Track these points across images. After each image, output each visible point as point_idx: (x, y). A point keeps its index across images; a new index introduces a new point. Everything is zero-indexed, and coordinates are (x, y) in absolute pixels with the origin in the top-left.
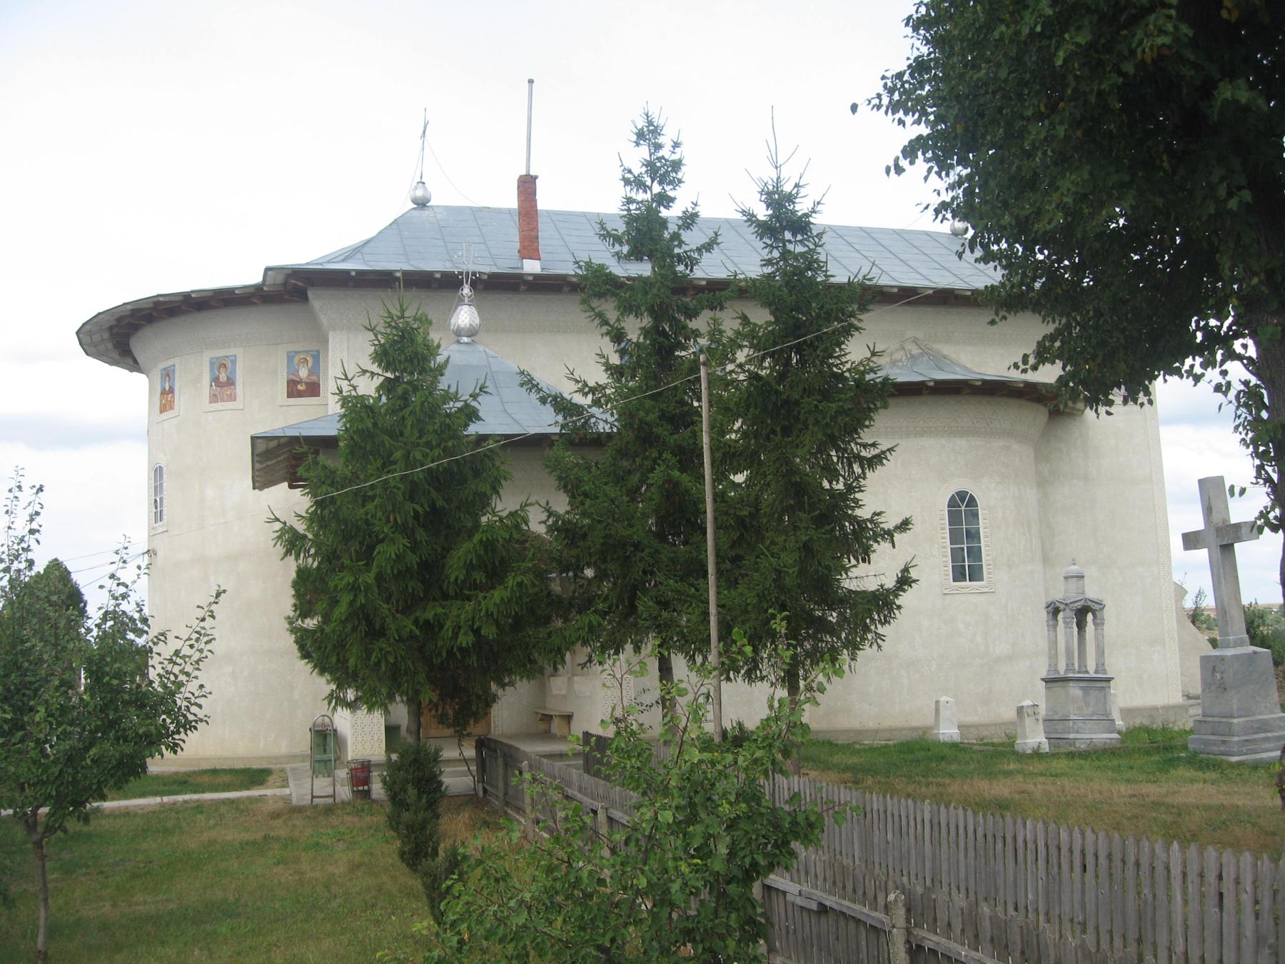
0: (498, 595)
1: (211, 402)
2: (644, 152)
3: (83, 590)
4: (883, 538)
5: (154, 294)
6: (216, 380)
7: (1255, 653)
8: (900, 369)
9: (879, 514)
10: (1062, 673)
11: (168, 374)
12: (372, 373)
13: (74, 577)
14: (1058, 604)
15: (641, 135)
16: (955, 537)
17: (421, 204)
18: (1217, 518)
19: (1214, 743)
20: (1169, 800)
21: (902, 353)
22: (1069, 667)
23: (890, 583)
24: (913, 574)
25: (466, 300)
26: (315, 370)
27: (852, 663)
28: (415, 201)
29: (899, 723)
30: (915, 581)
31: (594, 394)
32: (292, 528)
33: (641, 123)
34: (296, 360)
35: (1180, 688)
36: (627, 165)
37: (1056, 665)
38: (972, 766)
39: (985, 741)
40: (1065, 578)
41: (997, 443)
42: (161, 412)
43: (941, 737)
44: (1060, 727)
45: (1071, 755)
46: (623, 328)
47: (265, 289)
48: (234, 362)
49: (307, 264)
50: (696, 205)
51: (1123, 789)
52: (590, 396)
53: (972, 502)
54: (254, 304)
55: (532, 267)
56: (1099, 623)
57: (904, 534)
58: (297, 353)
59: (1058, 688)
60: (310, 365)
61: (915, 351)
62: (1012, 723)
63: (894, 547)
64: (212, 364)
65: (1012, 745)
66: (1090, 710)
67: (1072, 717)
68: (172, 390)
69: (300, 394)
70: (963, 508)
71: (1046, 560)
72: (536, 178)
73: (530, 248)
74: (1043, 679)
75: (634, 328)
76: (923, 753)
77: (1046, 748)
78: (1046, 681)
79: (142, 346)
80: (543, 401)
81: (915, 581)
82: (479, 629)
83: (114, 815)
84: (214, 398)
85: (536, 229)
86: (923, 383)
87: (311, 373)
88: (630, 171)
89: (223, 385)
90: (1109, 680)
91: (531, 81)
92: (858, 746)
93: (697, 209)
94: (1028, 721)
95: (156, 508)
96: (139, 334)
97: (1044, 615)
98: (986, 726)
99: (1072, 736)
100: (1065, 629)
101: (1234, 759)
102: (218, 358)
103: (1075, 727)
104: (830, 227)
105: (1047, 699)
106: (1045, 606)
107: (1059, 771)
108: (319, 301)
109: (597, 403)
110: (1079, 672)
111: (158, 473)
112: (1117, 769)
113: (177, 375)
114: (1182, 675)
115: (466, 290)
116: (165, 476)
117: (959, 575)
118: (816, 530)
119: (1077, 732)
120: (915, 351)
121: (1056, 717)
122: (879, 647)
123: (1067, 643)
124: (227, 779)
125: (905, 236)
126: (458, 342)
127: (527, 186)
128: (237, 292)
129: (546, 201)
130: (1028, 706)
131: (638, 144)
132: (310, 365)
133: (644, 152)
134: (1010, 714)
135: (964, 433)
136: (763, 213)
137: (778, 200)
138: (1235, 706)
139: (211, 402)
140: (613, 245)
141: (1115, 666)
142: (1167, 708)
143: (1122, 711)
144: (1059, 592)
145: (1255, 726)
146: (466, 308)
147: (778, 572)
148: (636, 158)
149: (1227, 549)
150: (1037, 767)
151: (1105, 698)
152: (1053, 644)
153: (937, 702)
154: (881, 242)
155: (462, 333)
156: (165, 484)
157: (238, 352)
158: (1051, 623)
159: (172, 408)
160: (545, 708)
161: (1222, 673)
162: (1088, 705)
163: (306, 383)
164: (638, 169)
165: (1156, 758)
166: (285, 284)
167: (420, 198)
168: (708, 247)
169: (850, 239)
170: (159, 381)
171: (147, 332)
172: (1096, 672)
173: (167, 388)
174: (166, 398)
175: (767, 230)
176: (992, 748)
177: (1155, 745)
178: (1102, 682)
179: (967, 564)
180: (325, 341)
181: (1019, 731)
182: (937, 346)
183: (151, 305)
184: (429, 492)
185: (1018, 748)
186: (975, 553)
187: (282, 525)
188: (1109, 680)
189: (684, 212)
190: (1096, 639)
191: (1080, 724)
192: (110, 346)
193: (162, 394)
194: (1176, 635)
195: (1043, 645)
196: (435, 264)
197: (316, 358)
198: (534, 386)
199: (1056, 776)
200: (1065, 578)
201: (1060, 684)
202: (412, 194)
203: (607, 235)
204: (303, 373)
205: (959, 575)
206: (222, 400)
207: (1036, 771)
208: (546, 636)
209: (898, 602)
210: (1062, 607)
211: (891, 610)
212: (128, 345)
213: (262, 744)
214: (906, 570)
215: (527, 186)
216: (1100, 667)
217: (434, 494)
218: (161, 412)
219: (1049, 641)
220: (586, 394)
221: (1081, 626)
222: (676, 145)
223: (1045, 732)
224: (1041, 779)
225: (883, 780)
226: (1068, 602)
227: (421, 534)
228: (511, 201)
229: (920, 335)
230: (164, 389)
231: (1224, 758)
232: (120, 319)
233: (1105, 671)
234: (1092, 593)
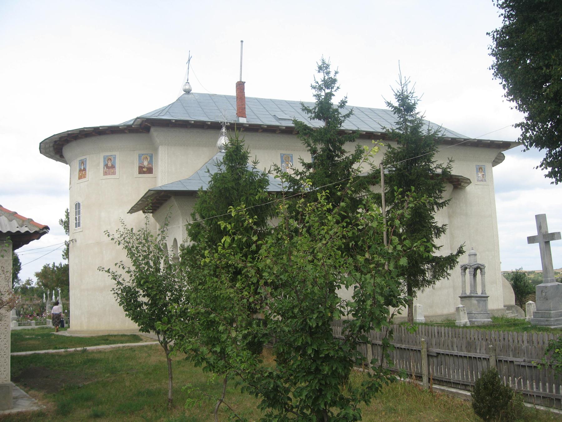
1: (104, 175)
3: (19, 258)
5: (83, 127)
6: (106, 165)
7: (559, 285)
9: (445, 225)
11: (83, 162)
15: (320, 68)
17: (188, 92)
18: (543, 230)
19: (543, 321)
23: (455, 253)
24: (464, 249)
26: (150, 162)
28: (185, 91)
31: (301, 175)
33: (320, 64)
34: (142, 157)
36: (317, 80)
40: (469, 255)
42: (79, 179)
43: (417, 321)
46: (316, 148)
47: (133, 126)
48: (115, 158)
49: (151, 116)
54: (125, 133)
55: (242, 120)
56: (482, 273)
58: (143, 155)
59: (466, 300)
60: (148, 160)
64: (104, 158)
67: (474, 312)
68: (85, 169)
69: (144, 173)
72: (245, 83)
73: (241, 112)
74: (459, 297)
75: (319, 147)
78: (461, 297)
79: (67, 152)
83: (93, 352)
84: (105, 173)
85: (244, 104)
87: (149, 163)
88: (317, 83)
89: (110, 168)
90: (487, 297)
91: (242, 42)
93: (347, 100)
95: (76, 221)
96: (69, 144)
101: (552, 327)
102: (107, 156)
104: (358, 108)
108: (155, 133)
109: (301, 178)
111: (78, 206)
113: (88, 162)
115: (224, 130)
116: (81, 207)
119: (475, 318)
122: (448, 278)
126: (220, 152)
127: (240, 86)
128: (120, 127)
129: (249, 93)
130: (461, 307)
131: (319, 72)
132: (148, 160)
136: (396, 104)
137: (403, 98)
138: (551, 306)
139: (104, 175)
145: (560, 314)
146: (223, 137)
148: (320, 77)
149: (547, 243)
152: (464, 282)
156: (81, 211)
157: (117, 154)
158: (463, 274)
159: (85, 177)
161: (546, 293)
163: (147, 168)
166: (140, 125)
167: (187, 89)
168: (348, 116)
169: (366, 113)
170: (78, 166)
171: (74, 144)
172: (482, 294)
173: (82, 168)
174: (82, 174)
175: (397, 110)
178: (484, 298)
180: (156, 150)
183: (78, 132)
188: (487, 297)
189: (341, 101)
191: (476, 315)
192: (52, 149)
194: (501, 280)
197: (151, 157)
198: (279, 171)
200: (469, 255)
201: (468, 298)
202: (184, 87)
203: (305, 109)
204: (146, 163)
206: (109, 174)
209: (458, 260)
210: (468, 267)
211: (454, 263)
212: (62, 149)
213: (127, 324)
214: (461, 247)
215: (240, 86)
216: (483, 291)
218: (79, 179)
220: (297, 175)
222: (336, 73)
228: (232, 92)
230: (81, 169)
231: (549, 327)
232: (61, 138)
234: (479, 262)
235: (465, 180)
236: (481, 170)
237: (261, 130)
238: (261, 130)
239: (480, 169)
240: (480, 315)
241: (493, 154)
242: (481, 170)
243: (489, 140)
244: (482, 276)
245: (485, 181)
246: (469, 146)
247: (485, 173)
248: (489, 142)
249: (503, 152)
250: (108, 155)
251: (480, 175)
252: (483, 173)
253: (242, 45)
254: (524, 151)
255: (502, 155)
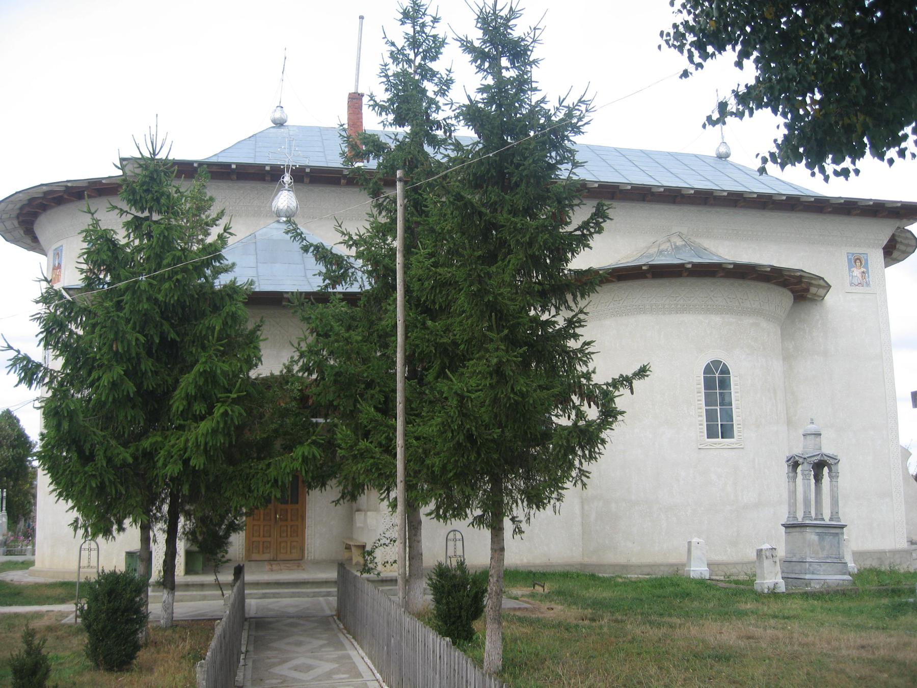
0: (205, 426)
2: (409, 28)
4: (622, 384)
8: (665, 256)
10: (800, 520)
12: (121, 210)
13: (22, 423)
14: (797, 458)
15: (406, 15)
16: (709, 401)
17: (279, 124)
20: (900, 656)
21: (668, 244)
22: (807, 514)
25: (287, 186)
27: (558, 504)
28: (274, 121)
29: (659, 559)
30: (622, 413)
32: (26, 358)
35: (905, 536)
37: (795, 512)
38: (711, 605)
39: (732, 578)
41: (748, 321)
44: (798, 567)
45: (806, 595)
50: (450, 71)
51: (852, 635)
52: (354, 248)
53: (725, 371)
56: (834, 476)
57: (642, 381)
59: (796, 533)
61: (679, 243)
62: (754, 563)
63: (632, 393)
65: (751, 582)
66: (825, 553)
68: (59, 267)
70: (717, 375)
71: (789, 423)
74: (783, 525)
76: (671, 589)
77: (782, 588)
78: (787, 526)
80: (306, 249)
81: (622, 413)
82: (189, 459)
86: (682, 265)
88: (393, 44)
90: (842, 527)
91: (362, 18)
92: (620, 580)
94: (767, 563)
97: (785, 468)
98: (735, 564)
99: (808, 577)
100: (804, 480)
103: (811, 568)
105: (787, 542)
106: (786, 459)
107: (792, 613)
110: (816, 519)
112: (848, 612)
114: (907, 524)
115: (287, 178)
117: (711, 434)
118: (507, 351)
119: (813, 573)
120: (679, 243)
121: (794, 559)
122: (584, 485)
123: (805, 492)
124: (59, 591)
125: (679, 157)
126: (278, 222)
130: (428, 594)
131: (403, 23)
133: (409, 28)
134: (753, 556)
135: (719, 311)
136: (476, 36)
140: (381, 114)
141: (849, 514)
142: (894, 552)
143: (854, 554)
144: (798, 449)
147: (461, 398)
150: (774, 607)
151: (839, 543)
152: (793, 493)
153: (690, 543)
154: (657, 160)
155: (282, 214)
158: (791, 475)
160: (351, 539)
162: (823, 549)
164: (401, 42)
165: (885, 601)
172: (831, 519)
173: (57, 265)
176: (733, 586)
177: (885, 587)
179: (719, 423)
181: (758, 572)
182: (698, 240)
184: (162, 325)
185: (757, 587)
186: (728, 415)
187: (16, 353)
188: (842, 527)
190: (832, 490)
191: (815, 566)
193: (53, 269)
195: (785, 495)
196: (265, 157)
199: (788, 618)
201: (798, 529)
205: (711, 434)
207: (770, 612)
208: (264, 467)
210: (801, 461)
216: (835, 515)
217: (166, 326)
219: (789, 492)
221: (818, 478)
223: (783, 572)
224: (772, 622)
225: (620, 618)
226: (806, 456)
227: (147, 365)
229: (684, 230)
233: (838, 519)
234: (828, 448)
235: (814, 279)
236: (858, 264)
237: (686, 274)
238: (686, 274)
239: (857, 260)
240: (824, 567)
241: (883, 231)
242: (858, 264)
243: (871, 200)
244: (831, 481)
245: (868, 285)
246: (830, 213)
247: (867, 269)
248: (871, 203)
249: (908, 228)
250: (398, 302)
251: (857, 272)
252: (863, 270)
253: (361, 24)
254: (685, 74)
255: (909, 235)
